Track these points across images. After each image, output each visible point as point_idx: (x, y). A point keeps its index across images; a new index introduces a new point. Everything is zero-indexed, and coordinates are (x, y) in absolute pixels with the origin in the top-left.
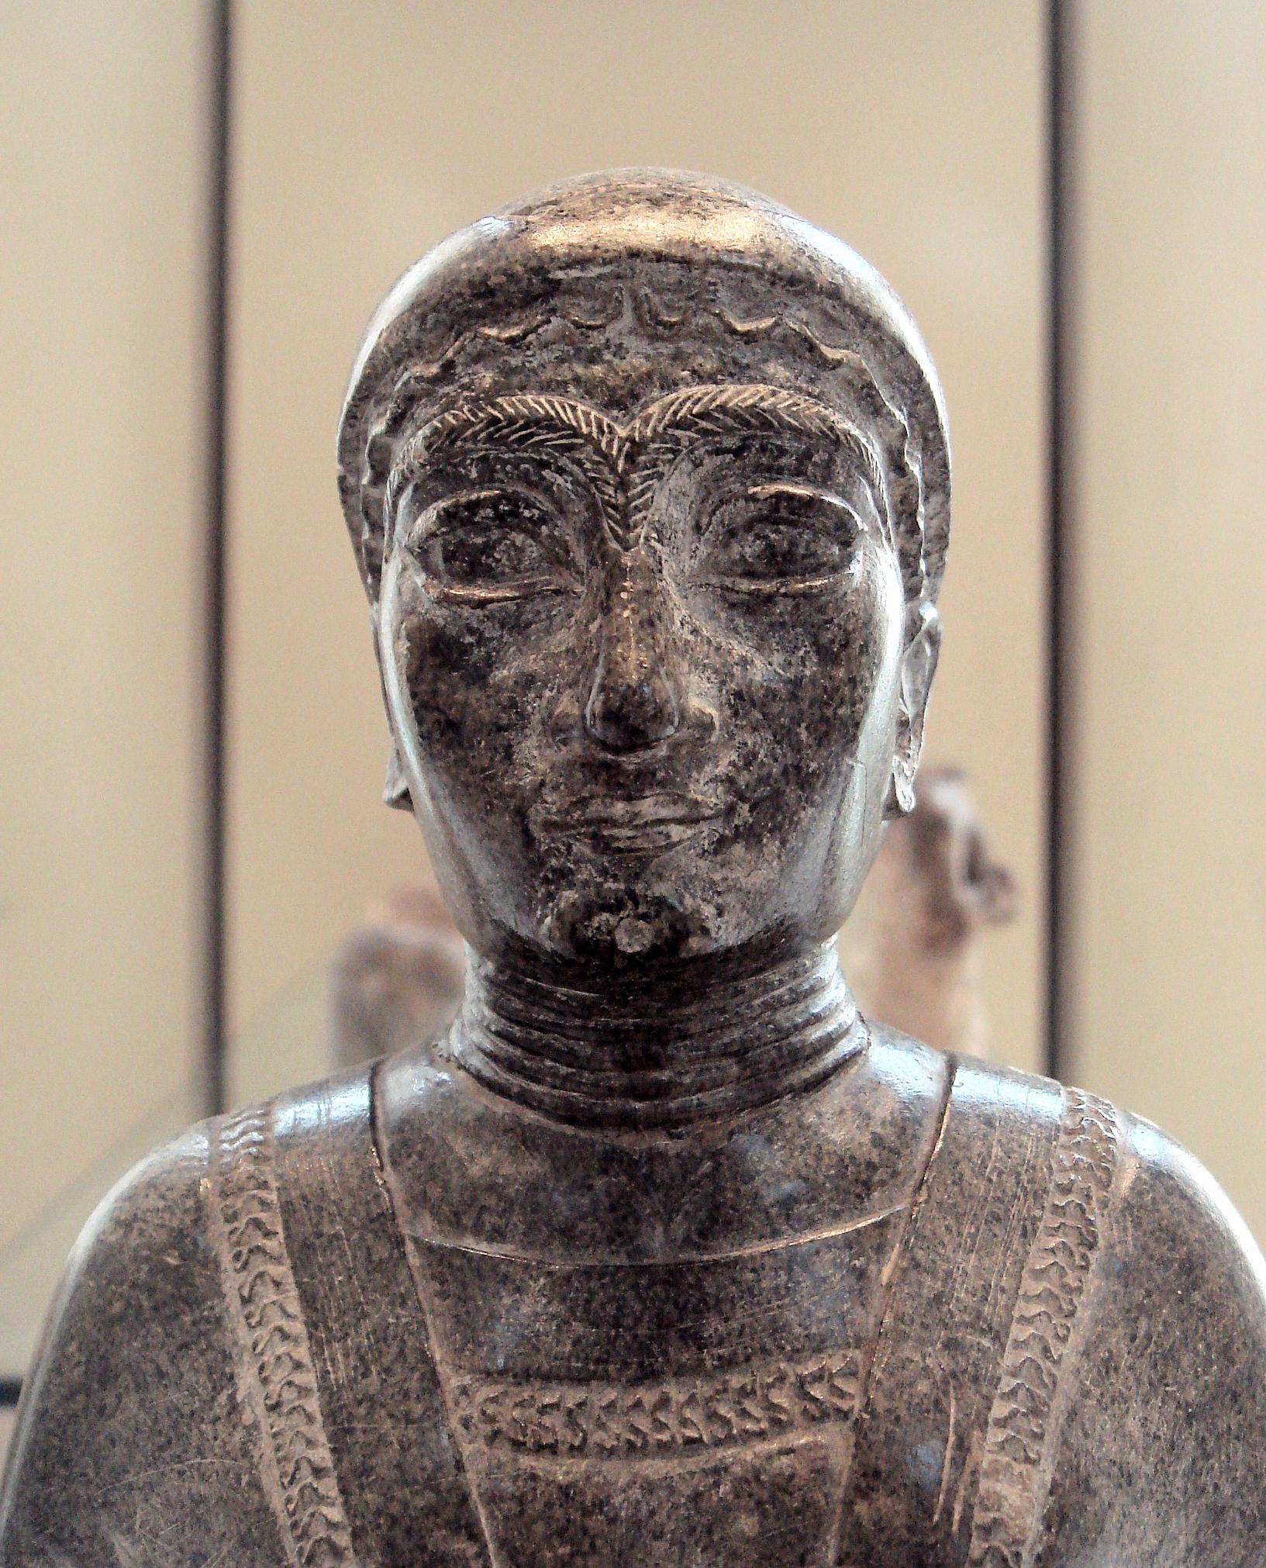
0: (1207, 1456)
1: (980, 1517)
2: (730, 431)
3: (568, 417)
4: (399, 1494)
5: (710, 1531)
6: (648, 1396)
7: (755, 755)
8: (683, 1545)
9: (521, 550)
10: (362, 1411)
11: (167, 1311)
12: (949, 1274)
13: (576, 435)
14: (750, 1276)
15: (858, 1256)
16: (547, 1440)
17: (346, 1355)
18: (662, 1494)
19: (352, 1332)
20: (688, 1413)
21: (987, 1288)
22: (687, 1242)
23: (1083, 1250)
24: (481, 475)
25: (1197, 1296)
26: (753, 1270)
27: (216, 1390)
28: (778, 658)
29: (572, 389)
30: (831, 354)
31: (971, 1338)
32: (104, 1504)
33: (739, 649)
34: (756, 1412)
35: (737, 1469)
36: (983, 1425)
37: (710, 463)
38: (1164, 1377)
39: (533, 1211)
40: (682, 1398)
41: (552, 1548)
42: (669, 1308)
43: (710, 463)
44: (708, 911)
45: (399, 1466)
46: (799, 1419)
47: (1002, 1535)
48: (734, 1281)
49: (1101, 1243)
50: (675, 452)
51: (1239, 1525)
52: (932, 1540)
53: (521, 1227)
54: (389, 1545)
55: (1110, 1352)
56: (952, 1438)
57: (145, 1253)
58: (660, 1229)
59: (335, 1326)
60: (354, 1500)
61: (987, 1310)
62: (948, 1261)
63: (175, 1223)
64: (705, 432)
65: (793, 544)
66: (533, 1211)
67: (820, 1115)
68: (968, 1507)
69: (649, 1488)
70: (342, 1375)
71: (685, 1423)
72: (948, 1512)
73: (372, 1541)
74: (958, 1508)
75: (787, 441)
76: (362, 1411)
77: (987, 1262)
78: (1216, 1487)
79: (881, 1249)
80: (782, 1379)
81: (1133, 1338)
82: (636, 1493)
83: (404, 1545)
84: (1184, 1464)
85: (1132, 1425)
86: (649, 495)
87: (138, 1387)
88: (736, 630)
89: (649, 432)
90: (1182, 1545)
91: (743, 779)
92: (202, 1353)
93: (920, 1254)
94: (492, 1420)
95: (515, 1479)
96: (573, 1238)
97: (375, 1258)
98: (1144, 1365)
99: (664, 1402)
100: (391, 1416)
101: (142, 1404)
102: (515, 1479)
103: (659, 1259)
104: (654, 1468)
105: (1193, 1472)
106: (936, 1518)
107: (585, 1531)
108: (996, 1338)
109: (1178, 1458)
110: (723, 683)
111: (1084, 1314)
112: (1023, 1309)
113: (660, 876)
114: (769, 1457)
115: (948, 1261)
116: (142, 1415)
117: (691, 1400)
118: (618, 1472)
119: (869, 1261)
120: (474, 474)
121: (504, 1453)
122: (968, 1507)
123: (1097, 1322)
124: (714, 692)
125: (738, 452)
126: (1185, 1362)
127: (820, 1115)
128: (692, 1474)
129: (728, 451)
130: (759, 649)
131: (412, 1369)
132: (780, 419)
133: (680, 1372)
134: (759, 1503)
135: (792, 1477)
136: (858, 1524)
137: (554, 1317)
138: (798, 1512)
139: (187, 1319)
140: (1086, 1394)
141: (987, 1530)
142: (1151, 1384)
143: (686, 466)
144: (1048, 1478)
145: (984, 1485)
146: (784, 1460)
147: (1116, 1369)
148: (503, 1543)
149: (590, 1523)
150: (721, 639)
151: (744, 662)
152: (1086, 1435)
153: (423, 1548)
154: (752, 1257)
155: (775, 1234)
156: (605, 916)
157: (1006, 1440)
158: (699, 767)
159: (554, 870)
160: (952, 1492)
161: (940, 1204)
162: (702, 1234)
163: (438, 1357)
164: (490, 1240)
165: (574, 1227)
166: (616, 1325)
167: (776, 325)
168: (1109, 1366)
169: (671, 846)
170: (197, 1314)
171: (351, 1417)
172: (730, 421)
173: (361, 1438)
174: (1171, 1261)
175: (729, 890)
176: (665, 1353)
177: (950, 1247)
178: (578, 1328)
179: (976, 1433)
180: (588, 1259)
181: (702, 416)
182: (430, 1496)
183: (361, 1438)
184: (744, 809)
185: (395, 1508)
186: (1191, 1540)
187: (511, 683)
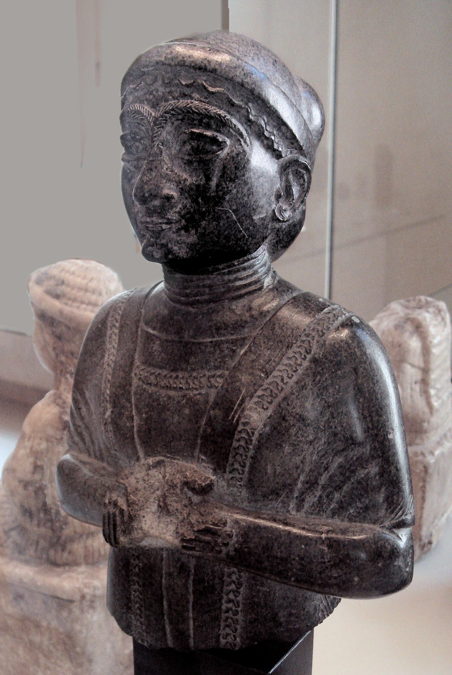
0: (333, 418)
1: (243, 420)
2: (179, 114)
6: (174, 375)
7: (186, 206)
9: (138, 147)
14: (204, 347)
15: (234, 346)
16: (149, 382)
18: (172, 400)
20: (182, 381)
22: (192, 337)
23: (306, 354)
25: (339, 372)
26: (205, 346)
28: (194, 179)
29: (145, 102)
30: (211, 89)
33: (185, 176)
34: (196, 383)
36: (252, 397)
37: (176, 123)
38: (322, 393)
40: (181, 376)
41: (145, 409)
43: (176, 123)
47: (249, 426)
48: (200, 348)
49: (313, 352)
50: (166, 121)
51: (342, 439)
55: (305, 384)
56: (241, 398)
58: (187, 332)
62: (261, 351)
64: (173, 115)
67: (237, 306)
68: (239, 417)
69: (169, 398)
71: (181, 383)
72: (233, 417)
74: (237, 416)
75: (195, 116)
77: (273, 353)
78: (336, 427)
79: (242, 346)
80: (204, 376)
81: (314, 381)
82: (165, 399)
84: (325, 419)
86: (159, 133)
88: (186, 171)
90: (323, 441)
91: (183, 213)
93: (253, 348)
94: (140, 375)
95: (141, 390)
98: (316, 389)
99: (177, 377)
102: (141, 390)
103: (186, 340)
104: (172, 393)
106: (230, 418)
109: (323, 417)
110: (178, 186)
111: (300, 372)
112: (281, 367)
113: (164, 238)
114: (195, 395)
115: (261, 351)
117: (183, 378)
118: (163, 392)
119: (237, 348)
121: (141, 383)
122: (239, 417)
123: (303, 374)
124: (175, 188)
125: (182, 120)
126: (331, 391)
127: (237, 306)
128: (179, 396)
129: (179, 120)
130: (190, 176)
132: (193, 111)
133: (182, 370)
134: (190, 406)
135: (199, 401)
140: (292, 394)
141: (245, 424)
142: (317, 395)
143: (170, 124)
144: (269, 414)
145: (246, 412)
146: (198, 396)
147: (306, 389)
148: (136, 405)
150: (181, 174)
151: (185, 180)
152: (288, 405)
154: (206, 342)
155: (214, 337)
157: (257, 402)
158: (172, 209)
160: (236, 412)
161: (264, 335)
163: (136, 358)
164: (153, 330)
167: (194, 82)
169: (163, 230)
172: (179, 111)
174: (333, 361)
175: (182, 243)
176: (180, 365)
177: (263, 348)
178: (163, 354)
179: (248, 398)
180: (169, 338)
184: (183, 221)
185: (117, 393)
186: (326, 440)
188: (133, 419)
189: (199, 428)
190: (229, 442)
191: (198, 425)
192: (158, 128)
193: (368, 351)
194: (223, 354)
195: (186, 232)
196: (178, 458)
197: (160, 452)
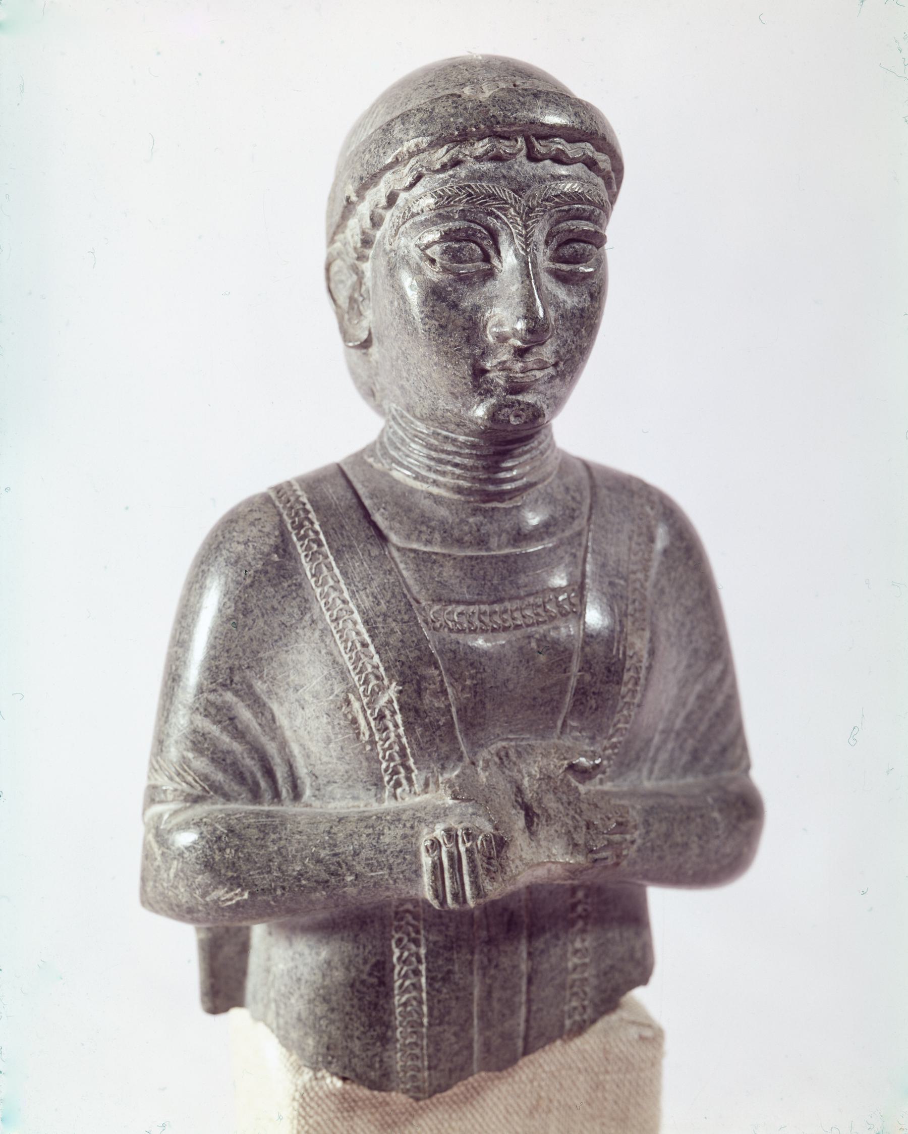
1: (630, 653)
3: (502, 195)
4: (403, 652)
5: (528, 662)
8: (517, 667)
10: (380, 619)
11: (274, 582)
12: (606, 554)
13: (506, 203)
17: (368, 597)
19: (368, 586)
21: (619, 560)
24: (460, 217)
27: (303, 614)
31: (617, 581)
32: (248, 667)
35: (537, 636)
39: (445, 532)
41: (469, 671)
42: (505, 572)
44: (545, 406)
45: (402, 641)
46: (559, 615)
52: (613, 661)
53: (439, 539)
54: (402, 674)
57: (259, 556)
58: (496, 539)
59: (359, 585)
60: (383, 656)
61: (620, 569)
63: (272, 542)
65: (584, 250)
66: (445, 532)
68: (625, 647)
70: (367, 604)
73: (393, 671)
76: (380, 619)
83: (408, 672)
85: (670, 616)
87: (263, 615)
89: (535, 203)
92: (294, 599)
96: (463, 543)
97: (373, 554)
100: (394, 620)
101: (265, 622)
105: (689, 635)
107: (481, 663)
108: (626, 580)
116: (266, 628)
120: (457, 217)
131: (400, 601)
136: (586, 656)
137: (458, 577)
138: (563, 652)
139: (285, 585)
149: (482, 660)
153: (416, 673)
156: (506, 409)
159: (484, 389)
162: (515, 541)
164: (426, 545)
165: (462, 539)
166: (484, 579)
168: (662, 592)
170: (290, 582)
171: (375, 622)
173: (382, 631)
178: (469, 582)
181: (556, 196)
182: (417, 653)
183: (382, 631)
185: (403, 658)
187: (469, 309)
188: (447, 694)
189: (569, 678)
190: (617, 687)
191: (568, 674)
192: (533, 223)
193: (555, 570)
194: (260, 615)
195: (561, 380)
196: (528, 736)
197: (498, 735)
